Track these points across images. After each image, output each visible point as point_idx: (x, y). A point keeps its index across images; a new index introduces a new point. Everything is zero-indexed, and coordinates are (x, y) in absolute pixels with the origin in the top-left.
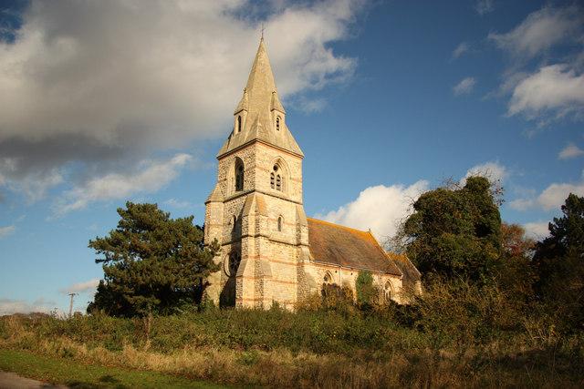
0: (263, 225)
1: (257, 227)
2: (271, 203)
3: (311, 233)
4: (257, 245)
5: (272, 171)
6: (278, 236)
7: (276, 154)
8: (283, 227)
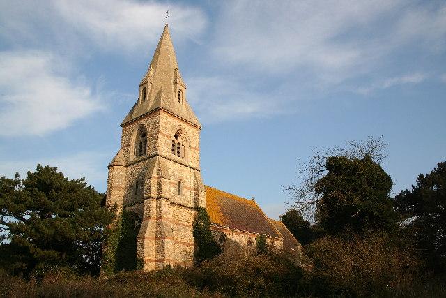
0: (165, 187)
1: (159, 189)
2: (172, 168)
3: (207, 197)
4: (159, 206)
5: (174, 138)
6: (179, 199)
7: (177, 123)
8: (183, 191)
